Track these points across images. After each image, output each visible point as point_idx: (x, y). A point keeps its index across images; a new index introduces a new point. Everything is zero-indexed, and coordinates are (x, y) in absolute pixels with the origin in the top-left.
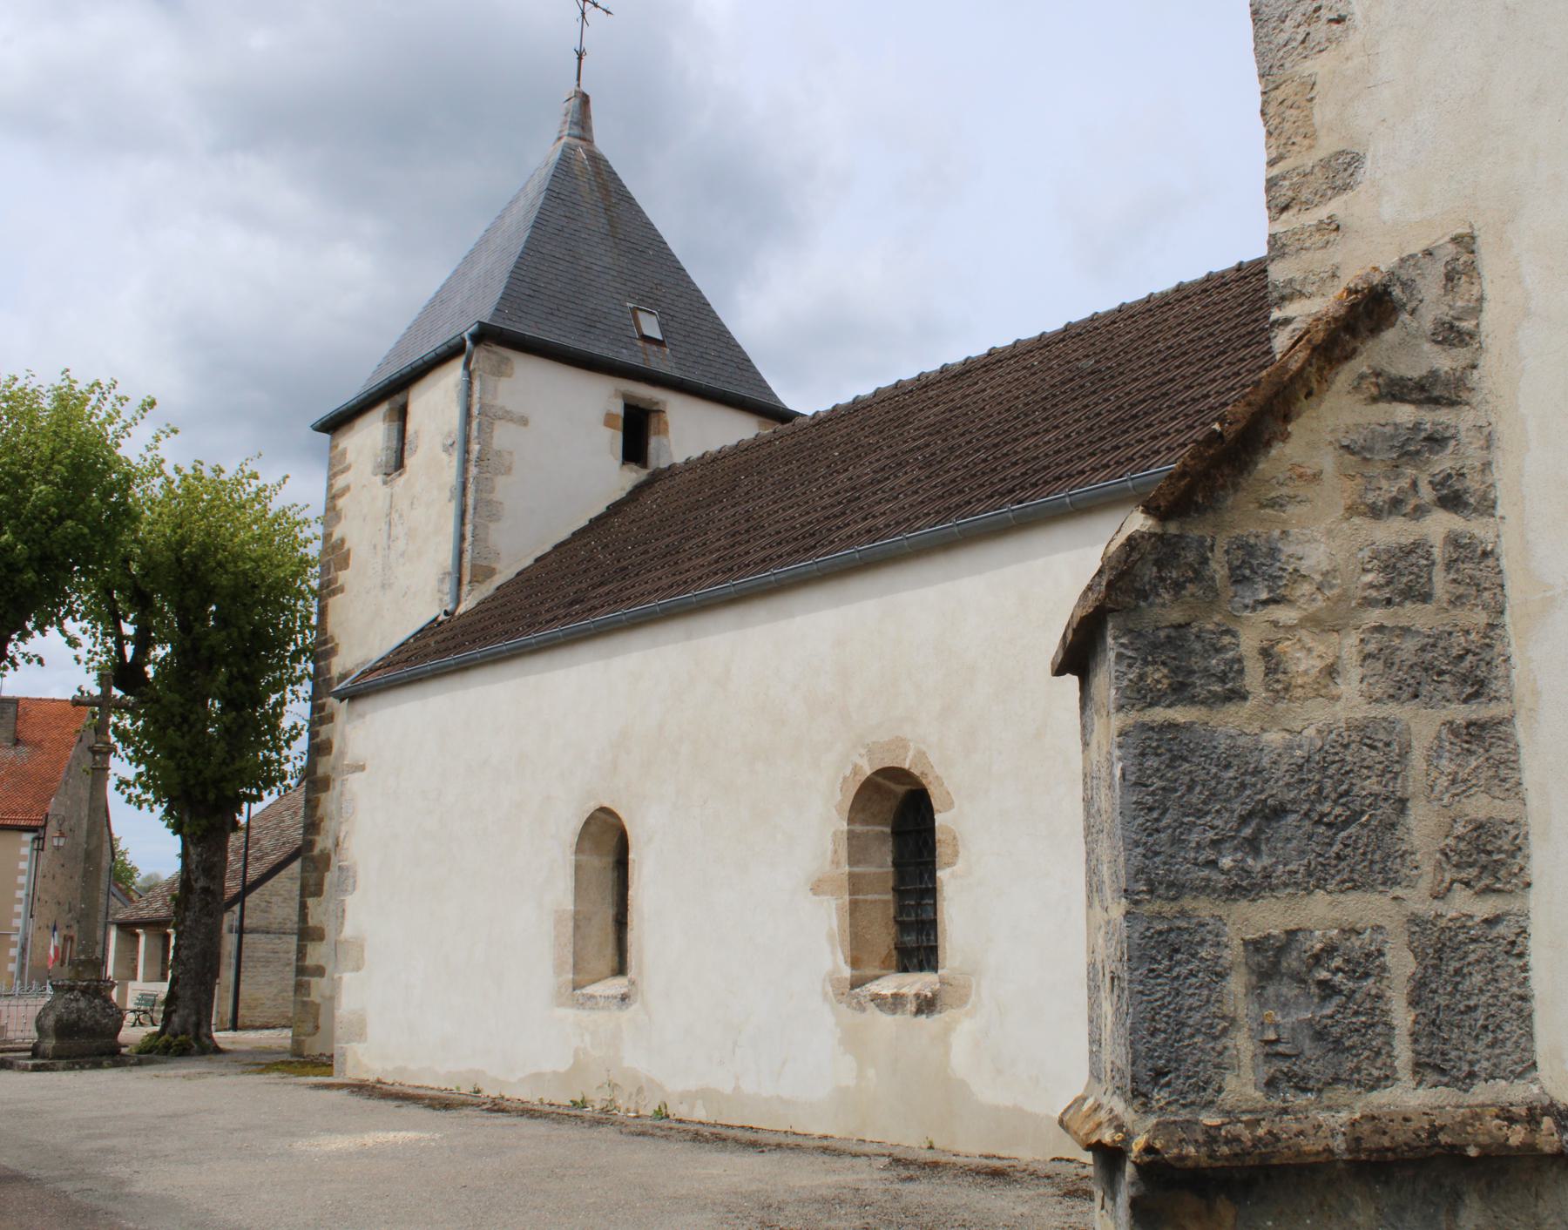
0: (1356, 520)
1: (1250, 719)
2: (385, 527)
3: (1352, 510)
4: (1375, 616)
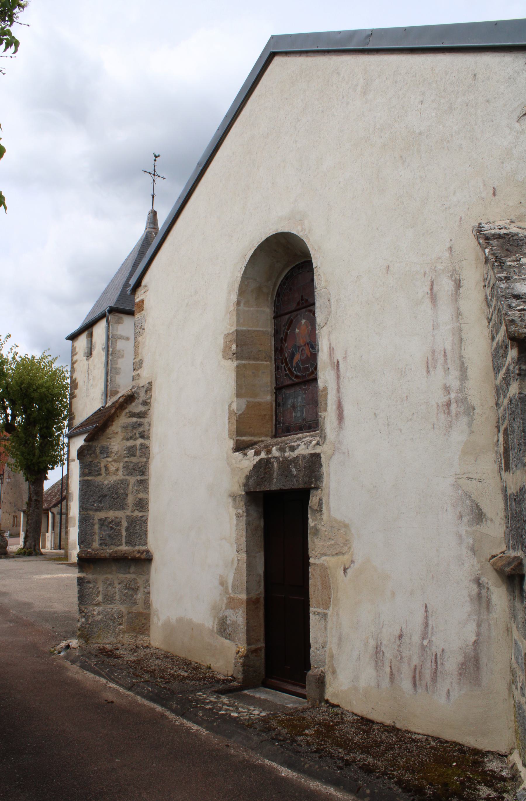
0: (124, 441)
1: (102, 479)
2: (87, 375)
3: (123, 439)
4: (126, 459)
